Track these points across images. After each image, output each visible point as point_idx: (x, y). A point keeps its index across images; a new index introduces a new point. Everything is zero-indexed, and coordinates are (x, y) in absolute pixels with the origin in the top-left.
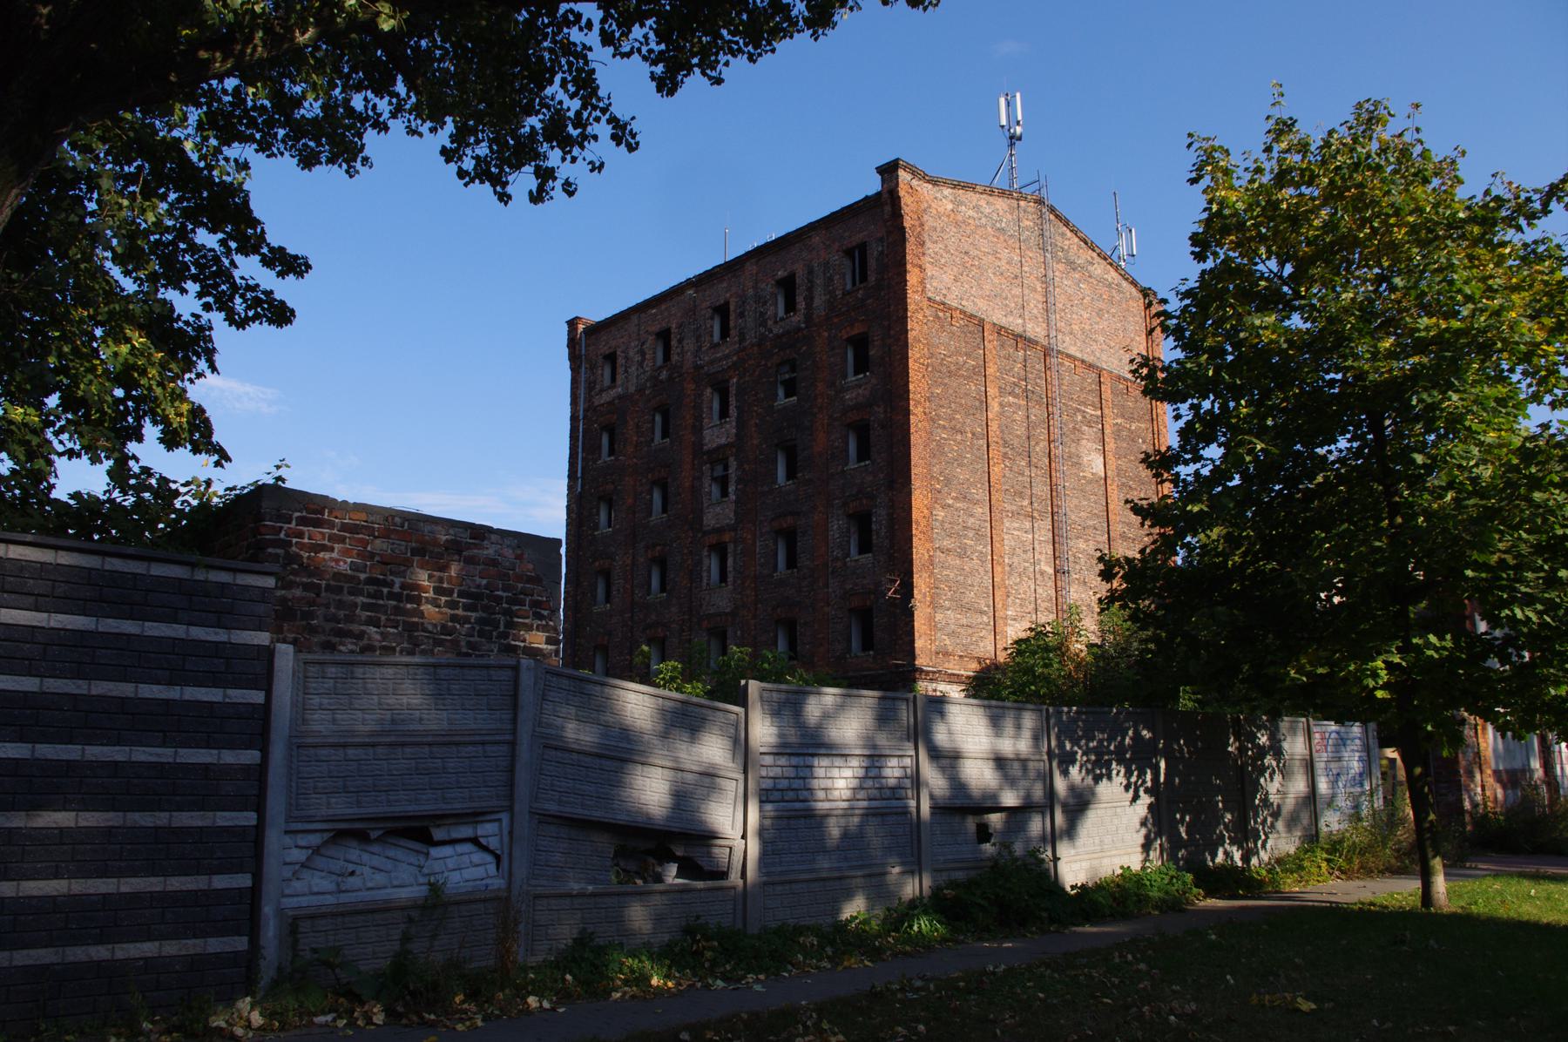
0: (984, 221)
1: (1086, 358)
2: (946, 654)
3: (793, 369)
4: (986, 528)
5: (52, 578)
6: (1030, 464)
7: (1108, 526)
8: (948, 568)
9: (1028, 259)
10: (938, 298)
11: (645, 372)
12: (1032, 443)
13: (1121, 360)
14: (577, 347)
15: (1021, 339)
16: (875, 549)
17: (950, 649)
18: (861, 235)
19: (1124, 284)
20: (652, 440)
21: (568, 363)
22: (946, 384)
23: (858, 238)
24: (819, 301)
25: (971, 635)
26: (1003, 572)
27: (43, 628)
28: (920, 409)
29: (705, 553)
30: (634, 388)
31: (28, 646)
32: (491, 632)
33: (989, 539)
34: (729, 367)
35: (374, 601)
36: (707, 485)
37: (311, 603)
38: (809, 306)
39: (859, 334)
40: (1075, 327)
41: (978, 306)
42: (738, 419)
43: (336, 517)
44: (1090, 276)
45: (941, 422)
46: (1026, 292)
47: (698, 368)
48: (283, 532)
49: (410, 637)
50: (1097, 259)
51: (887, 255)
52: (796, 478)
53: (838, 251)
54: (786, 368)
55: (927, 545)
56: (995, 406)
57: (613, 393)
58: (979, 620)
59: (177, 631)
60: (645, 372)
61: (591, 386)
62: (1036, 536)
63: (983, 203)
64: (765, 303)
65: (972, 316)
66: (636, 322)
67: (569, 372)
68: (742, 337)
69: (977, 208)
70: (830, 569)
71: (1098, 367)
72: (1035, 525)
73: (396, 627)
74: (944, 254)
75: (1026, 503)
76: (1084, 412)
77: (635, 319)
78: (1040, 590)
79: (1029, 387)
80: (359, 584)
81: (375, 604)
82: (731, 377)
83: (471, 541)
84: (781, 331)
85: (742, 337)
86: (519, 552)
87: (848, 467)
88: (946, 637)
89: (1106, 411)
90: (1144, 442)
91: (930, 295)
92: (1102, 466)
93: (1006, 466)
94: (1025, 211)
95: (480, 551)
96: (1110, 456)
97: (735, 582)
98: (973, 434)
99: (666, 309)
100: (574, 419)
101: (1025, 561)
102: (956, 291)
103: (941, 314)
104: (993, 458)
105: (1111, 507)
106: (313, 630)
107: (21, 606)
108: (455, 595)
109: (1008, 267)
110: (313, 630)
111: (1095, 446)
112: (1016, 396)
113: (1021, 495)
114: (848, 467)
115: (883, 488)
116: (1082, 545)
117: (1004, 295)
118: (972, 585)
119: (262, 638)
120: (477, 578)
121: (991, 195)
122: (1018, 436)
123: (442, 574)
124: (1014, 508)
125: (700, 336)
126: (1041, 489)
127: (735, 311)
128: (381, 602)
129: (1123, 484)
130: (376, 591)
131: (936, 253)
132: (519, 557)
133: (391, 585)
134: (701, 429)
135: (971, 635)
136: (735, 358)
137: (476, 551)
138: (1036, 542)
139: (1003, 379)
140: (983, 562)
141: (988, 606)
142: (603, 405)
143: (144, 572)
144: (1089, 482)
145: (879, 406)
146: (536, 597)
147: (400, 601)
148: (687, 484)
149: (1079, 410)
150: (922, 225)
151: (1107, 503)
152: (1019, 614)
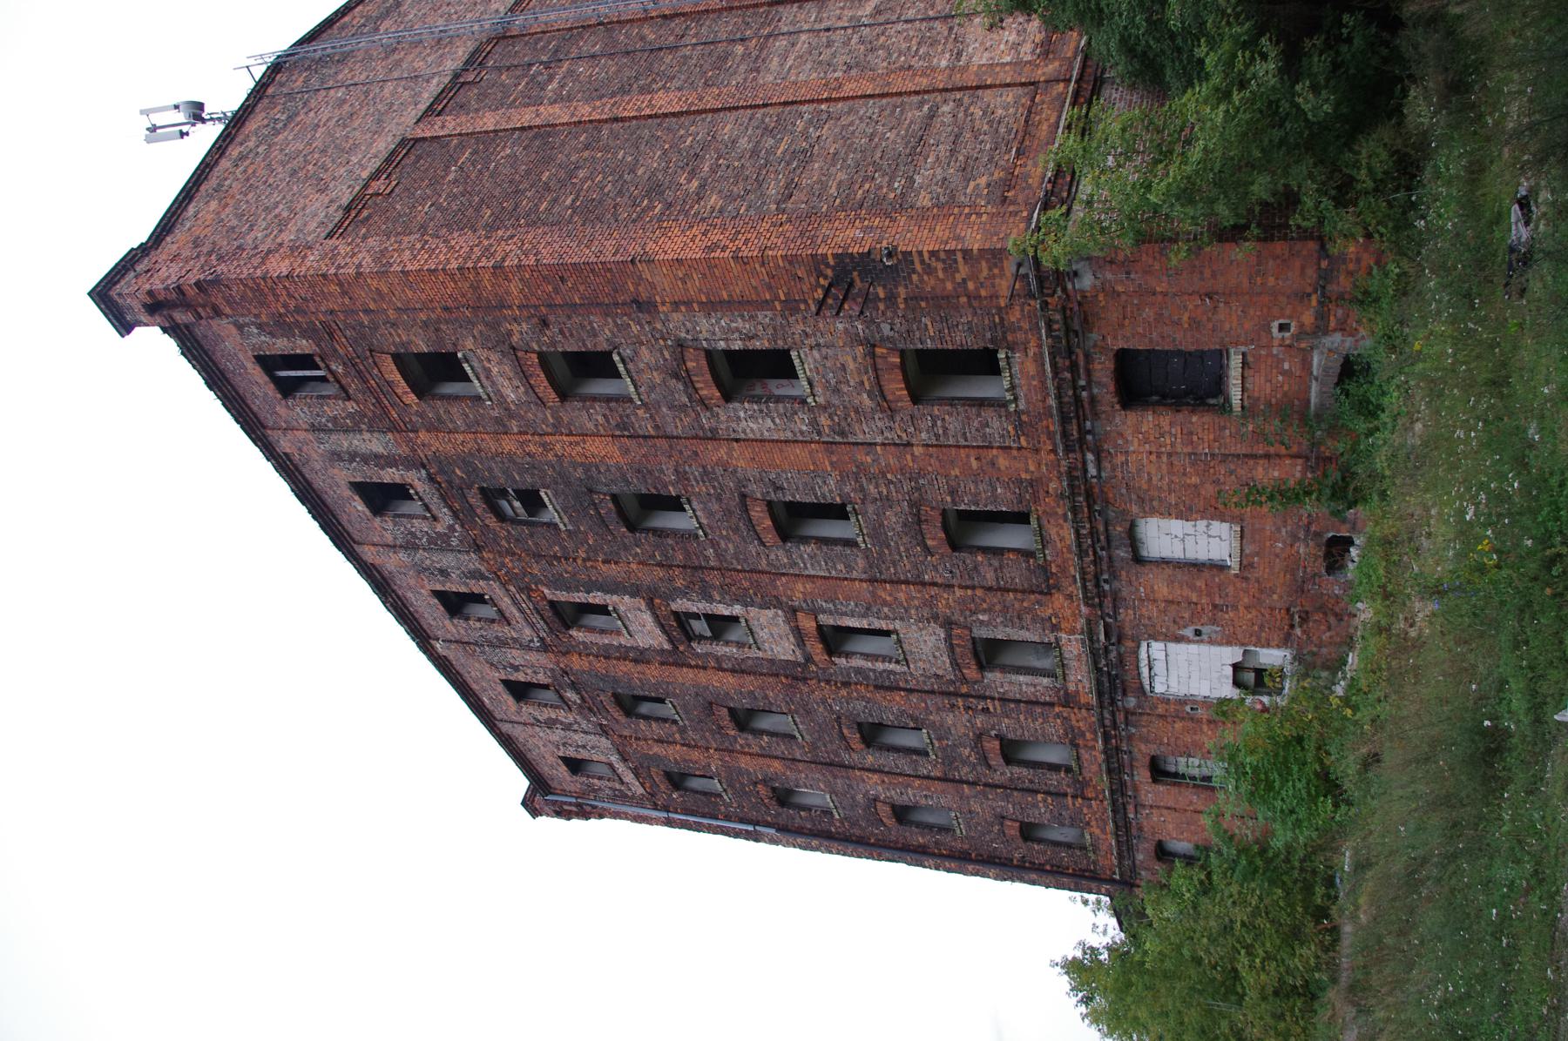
2: (1009, 182)
3: (503, 493)
6: (673, 49)
8: (824, 187)
14: (566, 807)
17: (998, 175)
24: (375, 444)
25: (976, 133)
29: (842, 662)
38: (390, 461)
45: (542, 208)
58: (948, 119)
65: (388, 161)
68: (476, 575)
70: (838, 439)
72: (785, 29)
74: (277, 211)
75: (739, 49)
77: (505, 728)
78: (911, 14)
85: (476, 575)
97: (887, 617)
98: (587, 147)
100: (669, 823)
101: (846, 43)
104: (640, 109)
112: (551, 79)
114: (635, 397)
115: (659, 326)
134: (642, 651)
135: (976, 133)
138: (817, 27)
140: (829, 117)
141: (922, 103)
148: (731, 680)
152: (950, 46)
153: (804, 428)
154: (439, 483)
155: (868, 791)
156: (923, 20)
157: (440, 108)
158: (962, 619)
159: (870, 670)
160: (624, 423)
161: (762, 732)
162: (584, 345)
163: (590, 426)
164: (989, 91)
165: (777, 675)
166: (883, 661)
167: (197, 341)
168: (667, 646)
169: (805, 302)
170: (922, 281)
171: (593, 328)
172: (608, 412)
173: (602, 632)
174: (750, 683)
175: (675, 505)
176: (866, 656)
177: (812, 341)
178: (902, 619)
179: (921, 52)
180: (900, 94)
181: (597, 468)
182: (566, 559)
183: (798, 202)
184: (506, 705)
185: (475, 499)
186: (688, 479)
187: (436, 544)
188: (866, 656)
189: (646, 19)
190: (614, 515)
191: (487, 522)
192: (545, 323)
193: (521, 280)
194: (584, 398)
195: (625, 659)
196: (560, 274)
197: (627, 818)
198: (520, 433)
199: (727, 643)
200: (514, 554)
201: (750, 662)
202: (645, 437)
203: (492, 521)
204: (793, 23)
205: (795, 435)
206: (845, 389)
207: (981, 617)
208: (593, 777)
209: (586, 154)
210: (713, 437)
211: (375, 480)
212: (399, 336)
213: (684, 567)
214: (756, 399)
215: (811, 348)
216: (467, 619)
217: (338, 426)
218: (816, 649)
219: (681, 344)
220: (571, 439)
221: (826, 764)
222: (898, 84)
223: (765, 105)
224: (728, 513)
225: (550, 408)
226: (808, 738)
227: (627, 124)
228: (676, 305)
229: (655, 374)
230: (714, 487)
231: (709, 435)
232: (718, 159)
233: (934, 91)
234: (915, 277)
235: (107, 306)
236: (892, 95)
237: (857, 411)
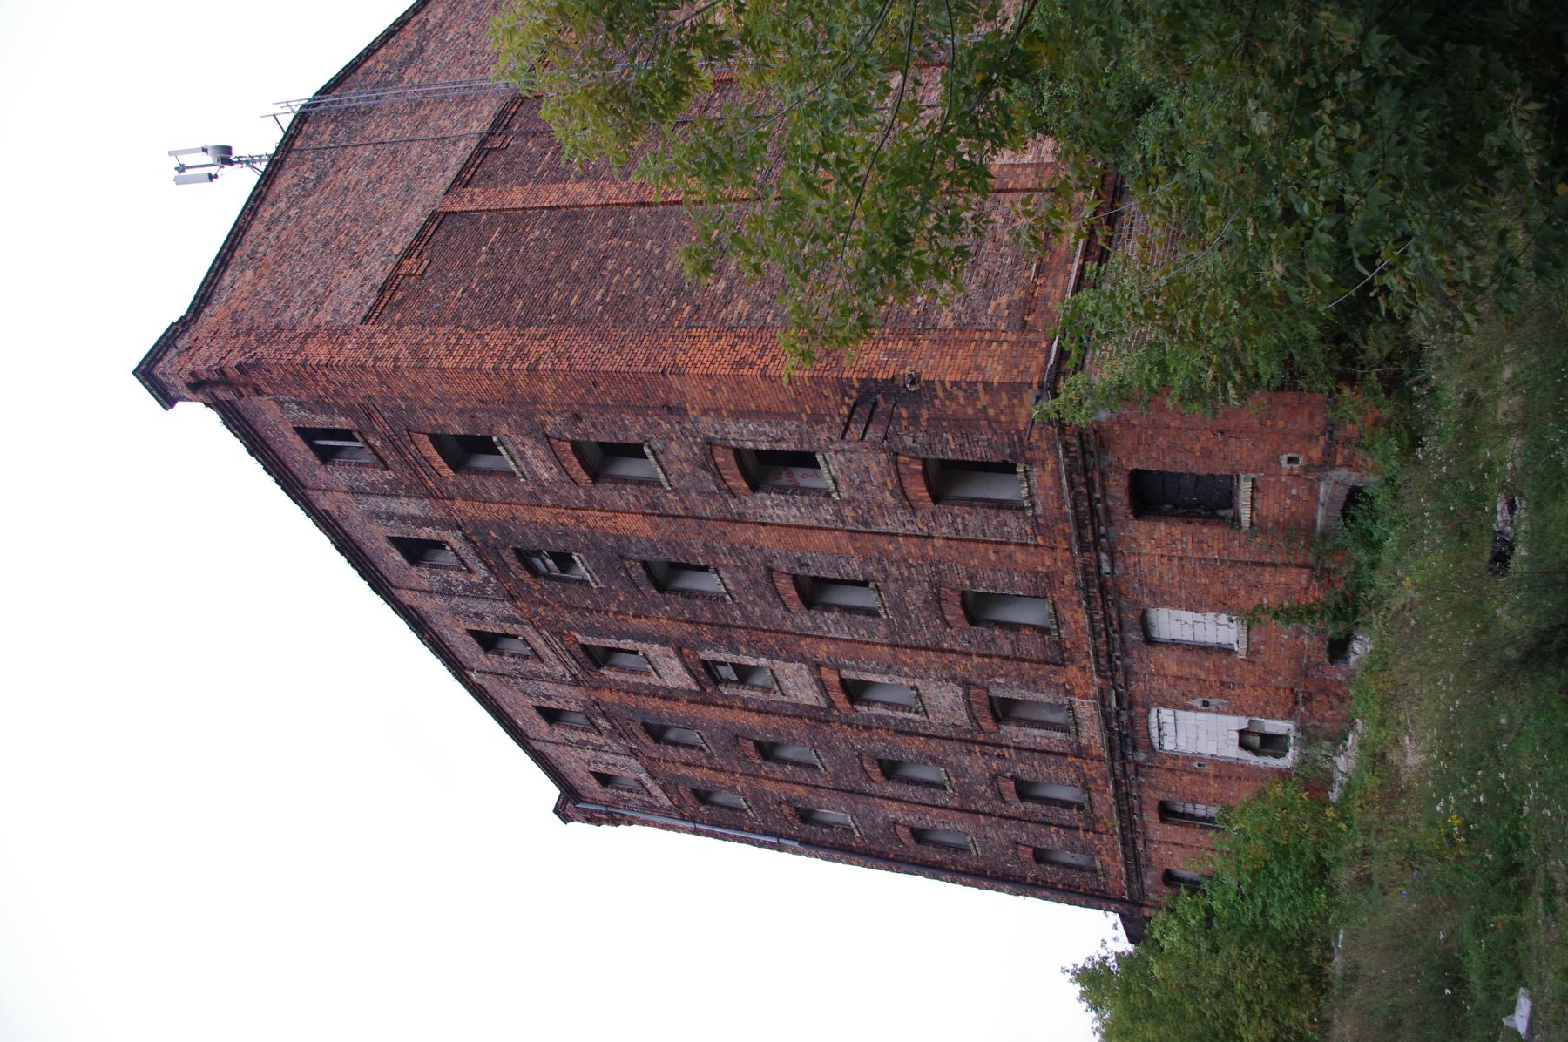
2: (1029, 304)
16: (806, 447)
17: (1019, 294)
24: (413, 507)
65: (419, 236)
68: (511, 620)
88: (993, 304)
97: (906, 675)
98: (615, 234)
100: (696, 832)
103: (399, 295)
104: (666, 194)
109: (374, 168)
115: (688, 426)
121: (264, 199)
162: (616, 437)
163: (622, 504)
171: (624, 424)
176: (888, 705)
192: (578, 417)
198: (553, 506)
199: (753, 687)
202: (675, 516)
203: (526, 577)
206: (869, 487)
209: (614, 241)
210: (741, 520)
214: (783, 490)
215: (836, 452)
219: (710, 443)
220: (603, 514)
226: (830, 769)
227: (654, 209)
230: (741, 561)
234: (937, 402)
237: (880, 506)
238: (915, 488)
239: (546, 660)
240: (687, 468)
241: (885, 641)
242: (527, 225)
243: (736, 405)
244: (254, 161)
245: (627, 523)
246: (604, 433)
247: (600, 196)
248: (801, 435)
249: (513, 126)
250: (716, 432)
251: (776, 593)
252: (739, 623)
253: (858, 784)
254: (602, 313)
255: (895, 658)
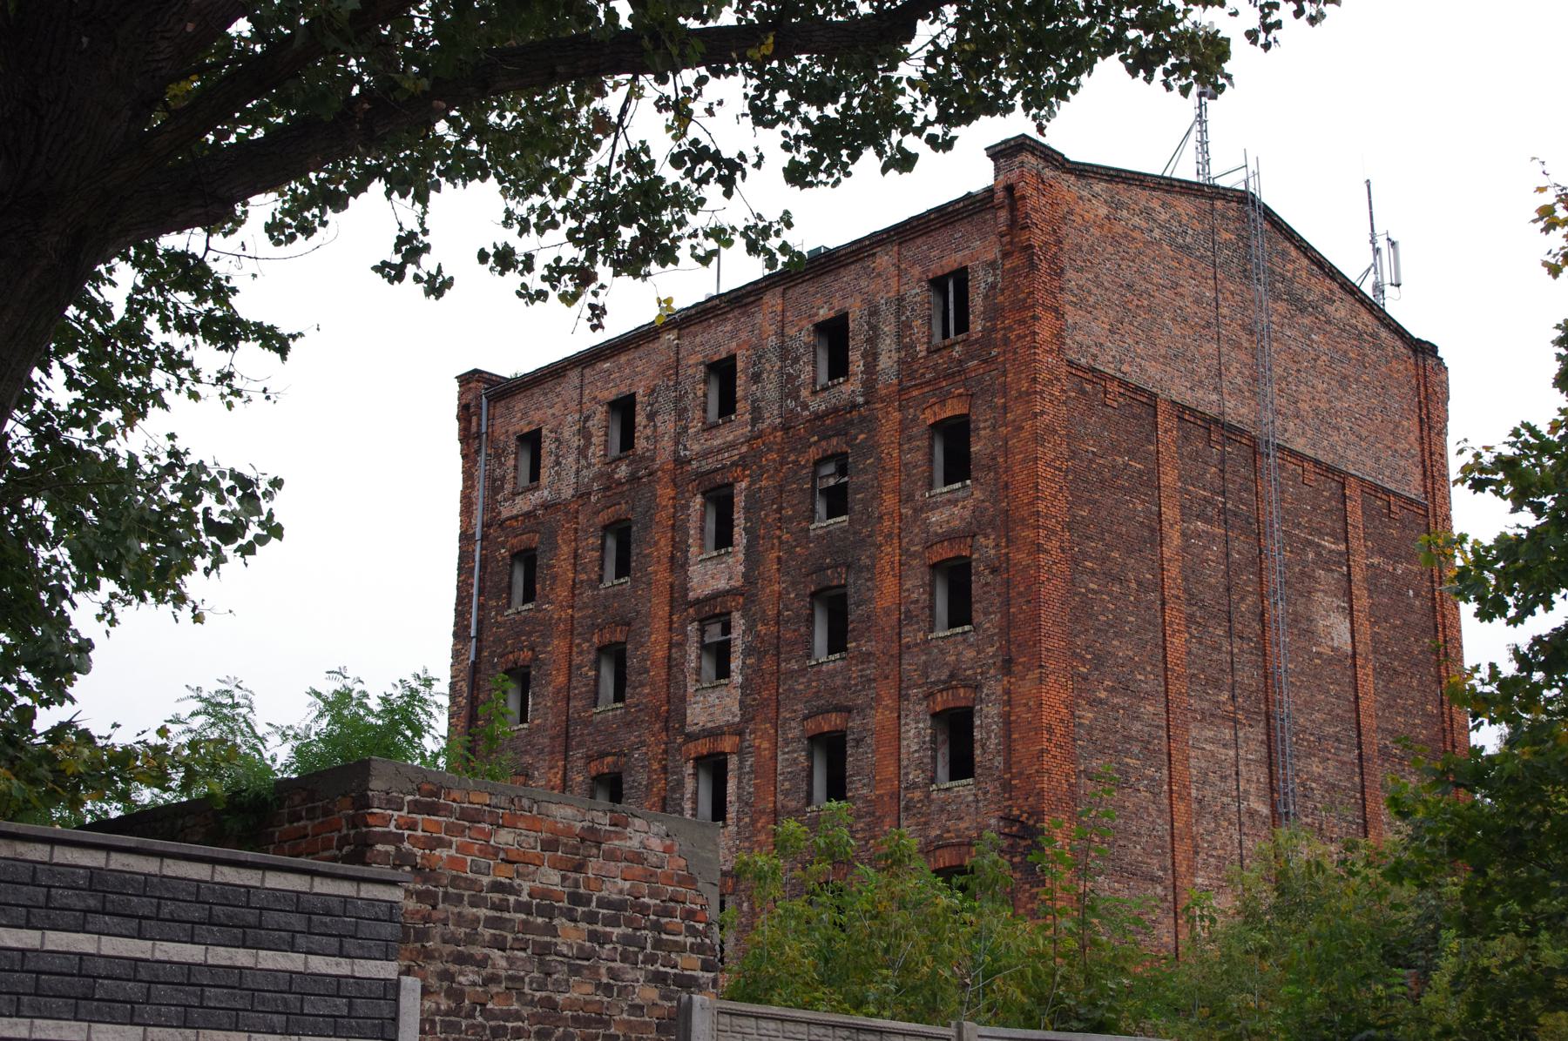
0: (1157, 233)
1: (1321, 456)
3: (842, 470)
4: (1160, 738)
5: (158, 894)
6: (1230, 633)
7: (1359, 735)
9: (1228, 294)
10: (1083, 361)
11: (589, 465)
12: (1235, 597)
13: (1378, 459)
14: (474, 419)
15: (1215, 426)
16: (978, 771)
18: (958, 256)
19: (1384, 333)
20: (601, 579)
21: (458, 445)
22: (1096, 502)
23: (952, 261)
26: (1188, 812)
27: (146, 960)
28: (1055, 543)
29: (689, 769)
30: (571, 492)
31: (131, 984)
32: (636, 954)
33: (1165, 757)
34: (733, 464)
35: (499, 914)
36: (693, 657)
37: (426, 919)
38: (871, 368)
39: (955, 417)
40: (1304, 406)
41: (1150, 373)
42: (749, 548)
43: (454, 801)
44: (1328, 322)
46: (1225, 349)
47: (680, 462)
48: (393, 822)
49: (542, 963)
50: (1339, 293)
51: (1002, 290)
52: (846, 649)
53: (920, 280)
54: (829, 469)
55: (1067, 767)
56: (1174, 539)
57: (535, 498)
59: (292, 962)
60: (589, 465)
61: (494, 486)
62: (1241, 752)
63: (1155, 204)
64: (796, 360)
65: (1137, 389)
66: (577, 382)
67: (459, 461)
69: (1147, 213)
70: (903, 804)
71: (1341, 471)
72: (1241, 734)
73: (524, 950)
74: (1094, 290)
75: (1224, 697)
76: (1319, 545)
77: (573, 376)
78: (1248, 843)
79: (1228, 506)
80: (481, 891)
81: (500, 918)
82: (736, 480)
83: (612, 828)
84: (823, 407)
85: (756, 419)
86: (668, 842)
87: (934, 635)
89: (1354, 544)
90: (1417, 595)
91: (1072, 356)
92: (1348, 635)
93: (1192, 636)
94: (1223, 217)
95: (622, 843)
96: (1361, 617)
97: (739, 820)
98: (1139, 584)
99: (628, 362)
100: (465, 537)
101: (1223, 793)
102: (1112, 349)
103: (1088, 387)
104: (1171, 623)
105: (1363, 704)
106: (429, 955)
107: (124, 932)
108: (594, 904)
109: (1195, 308)
110: (429, 955)
111: (1336, 602)
112: (1208, 521)
113: (1218, 687)
114: (934, 635)
115: (992, 671)
116: (1317, 769)
117: (1189, 354)
118: (1138, 834)
119: (386, 970)
120: (619, 880)
122: (1210, 586)
123: (578, 875)
124: (1206, 705)
125: (685, 410)
126: (1248, 676)
127: (745, 370)
128: (506, 915)
129: (1383, 666)
130: (501, 900)
131: (1080, 287)
132: (668, 850)
133: (518, 893)
134: (684, 565)
136: (744, 449)
137: (617, 842)
138: (1241, 763)
139: (1188, 492)
140: (1155, 795)
141: (1164, 869)
142: (515, 518)
143: (258, 885)
144: (1329, 661)
145: (986, 536)
146: (688, 905)
147: (529, 913)
149: (1310, 543)
150: (1059, 242)
151: (1357, 697)
152: (1215, 883)
153: (911, 777)
154: (850, 412)
155: (537, 769)
156: (1241, 855)
157: (1187, 417)
158: (742, 887)
159: (683, 795)
160: (912, 618)
161: (598, 670)
162: (977, 602)
163: (908, 585)
164: (1172, 921)
165: (668, 702)
166: (693, 809)
167: (980, 212)
168: (692, 595)
169: (1010, 799)
170: (1025, 891)
171: (991, 613)
172: (921, 605)
173: (702, 529)
174: (658, 673)
175: (837, 643)
176: (696, 793)
177: (981, 797)
178: (738, 833)
179: (1211, 860)
180: (1173, 851)
181: (870, 579)
182: (780, 519)
183: (1087, 786)
184: (608, 385)
185: (835, 444)
186: (862, 663)
187: (787, 383)
188: (696, 793)
189: (1262, 596)
190: (826, 583)
191: (813, 449)
192: (994, 571)
193: (1028, 566)
194: (932, 585)
195: (673, 546)
196: (1035, 601)
197: (465, 487)
198: (901, 515)
199: (699, 658)
200: (782, 465)
201: (681, 677)
202: (899, 634)
203: (813, 453)
204: (1247, 740)
205: (905, 767)
206: (944, 817)
207: (745, 904)
208: (516, 459)
209: (1134, 585)
210: (901, 696)
211: (851, 343)
212: (985, 428)
213: (778, 637)
214: (934, 740)
215: (975, 795)
216: (706, 382)
217: (903, 328)
218: (703, 747)
219: (978, 687)
220: (896, 565)
221: (567, 732)
222: (1182, 848)
223: (1169, 737)
224: (834, 692)
225: (923, 552)
226: (599, 718)
227: (1159, 614)
228: (1007, 692)
229: (954, 658)
230: (856, 685)
231: (903, 692)
232: (1123, 708)
233: (1175, 878)
234: (1027, 886)
235: (1011, 147)
236: (1173, 844)
237: (926, 823)
238: (947, 856)
239: (706, 435)
240: (951, 659)
241: (779, 805)
242: (1146, 495)
243: (1015, 721)
244: (1201, 124)
245: (889, 584)
246: (980, 591)
247: (1169, 561)
248: (990, 768)
249: (1230, 445)
250: (987, 695)
251: (825, 711)
252: (783, 665)
253: (579, 745)
254: (1080, 593)
255: (763, 812)
